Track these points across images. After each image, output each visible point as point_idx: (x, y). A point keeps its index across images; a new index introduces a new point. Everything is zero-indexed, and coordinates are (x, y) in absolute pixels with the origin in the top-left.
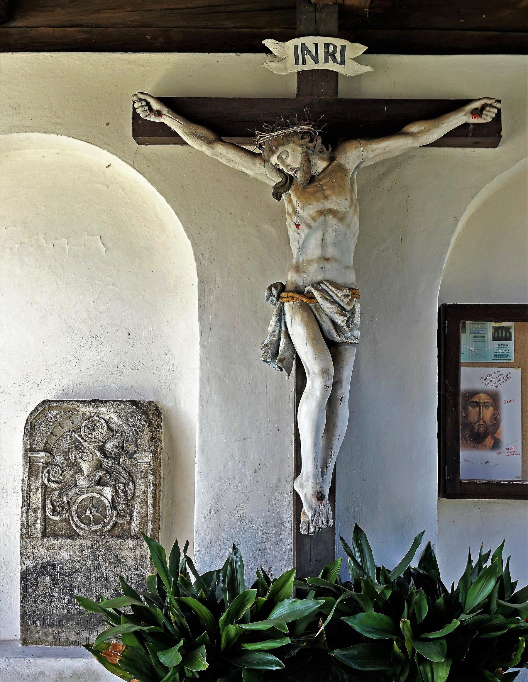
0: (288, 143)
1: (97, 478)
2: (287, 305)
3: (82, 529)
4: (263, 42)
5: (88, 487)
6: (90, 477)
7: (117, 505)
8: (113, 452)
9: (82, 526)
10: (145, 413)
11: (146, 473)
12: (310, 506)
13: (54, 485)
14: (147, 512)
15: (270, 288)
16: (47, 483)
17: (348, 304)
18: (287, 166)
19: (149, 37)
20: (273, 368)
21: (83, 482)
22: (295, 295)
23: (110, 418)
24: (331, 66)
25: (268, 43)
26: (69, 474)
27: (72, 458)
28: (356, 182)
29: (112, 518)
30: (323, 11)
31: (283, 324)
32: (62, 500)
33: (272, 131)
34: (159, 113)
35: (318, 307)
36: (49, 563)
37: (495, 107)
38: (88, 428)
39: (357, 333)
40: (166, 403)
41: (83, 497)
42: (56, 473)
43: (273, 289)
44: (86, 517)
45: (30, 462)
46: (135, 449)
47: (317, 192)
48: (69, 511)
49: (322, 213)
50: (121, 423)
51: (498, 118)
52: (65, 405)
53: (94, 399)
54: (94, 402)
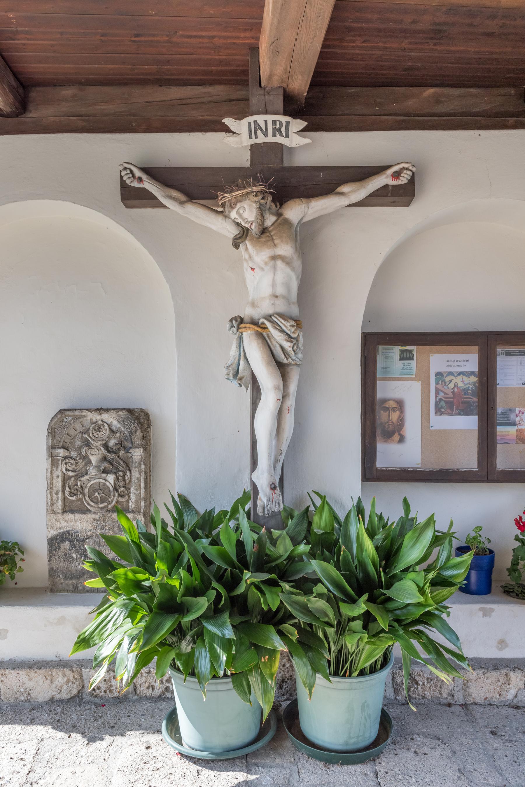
0: (245, 200)
1: (102, 468)
2: (245, 334)
3: (92, 506)
4: (223, 121)
5: (96, 475)
6: (98, 467)
7: (118, 487)
8: (114, 448)
9: (92, 504)
10: (138, 418)
11: (140, 464)
12: (265, 495)
13: (71, 474)
14: (140, 493)
15: (231, 321)
16: (65, 472)
17: (294, 332)
18: (244, 220)
19: (134, 124)
20: (235, 383)
21: (92, 471)
22: (251, 326)
23: (111, 422)
24: (279, 139)
25: (228, 121)
26: (81, 464)
27: (84, 453)
28: (298, 234)
29: (115, 499)
30: (271, 93)
31: (242, 349)
32: (77, 485)
33: (231, 192)
34: (140, 180)
35: (270, 335)
36: (68, 532)
37: (411, 171)
38: (95, 430)
39: (300, 356)
40: (153, 410)
41: (92, 482)
42: (72, 464)
43: (234, 321)
44: (95, 497)
45: (52, 456)
46: (130, 446)
47: (268, 241)
48: (82, 493)
49: (274, 258)
50: (119, 426)
51: (412, 181)
52: (77, 413)
53: (99, 407)
54: (99, 410)
